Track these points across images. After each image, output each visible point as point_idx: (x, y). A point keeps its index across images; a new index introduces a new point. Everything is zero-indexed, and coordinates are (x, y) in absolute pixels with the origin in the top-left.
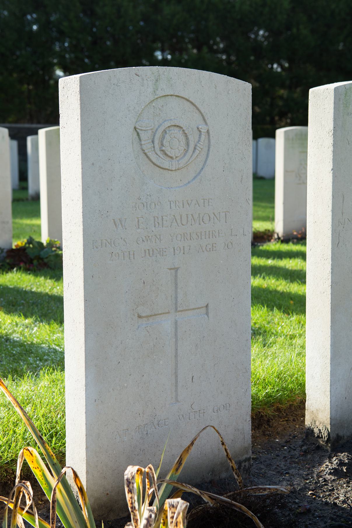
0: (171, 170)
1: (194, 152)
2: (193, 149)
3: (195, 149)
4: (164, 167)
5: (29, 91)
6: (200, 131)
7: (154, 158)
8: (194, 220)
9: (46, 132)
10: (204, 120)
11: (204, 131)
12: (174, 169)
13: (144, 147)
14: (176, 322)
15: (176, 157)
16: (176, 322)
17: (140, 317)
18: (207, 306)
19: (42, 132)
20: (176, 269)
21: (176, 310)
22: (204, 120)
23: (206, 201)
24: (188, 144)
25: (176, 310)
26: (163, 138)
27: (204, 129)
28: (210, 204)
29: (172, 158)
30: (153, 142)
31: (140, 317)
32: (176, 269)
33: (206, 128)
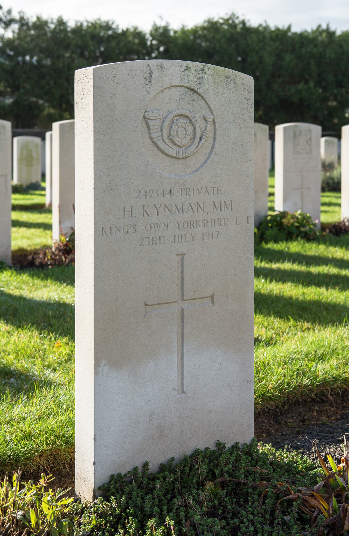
0: (179, 159)
1: (199, 143)
2: (199, 139)
3: (201, 140)
4: (169, 153)
5: (344, 467)
6: (206, 121)
7: (160, 143)
8: (178, 210)
9: (60, 125)
10: (211, 110)
11: (210, 120)
12: (181, 157)
13: (153, 136)
14: (183, 310)
15: (184, 146)
16: (183, 310)
17: (146, 305)
18: (212, 296)
19: (56, 126)
20: (183, 255)
21: (183, 300)
22: (211, 110)
23: (216, 189)
24: (194, 136)
25: (183, 300)
26: (171, 127)
27: (210, 118)
28: (219, 192)
29: (180, 147)
30: (161, 130)
31: (143, 206)
32: (183, 255)
33: (212, 117)
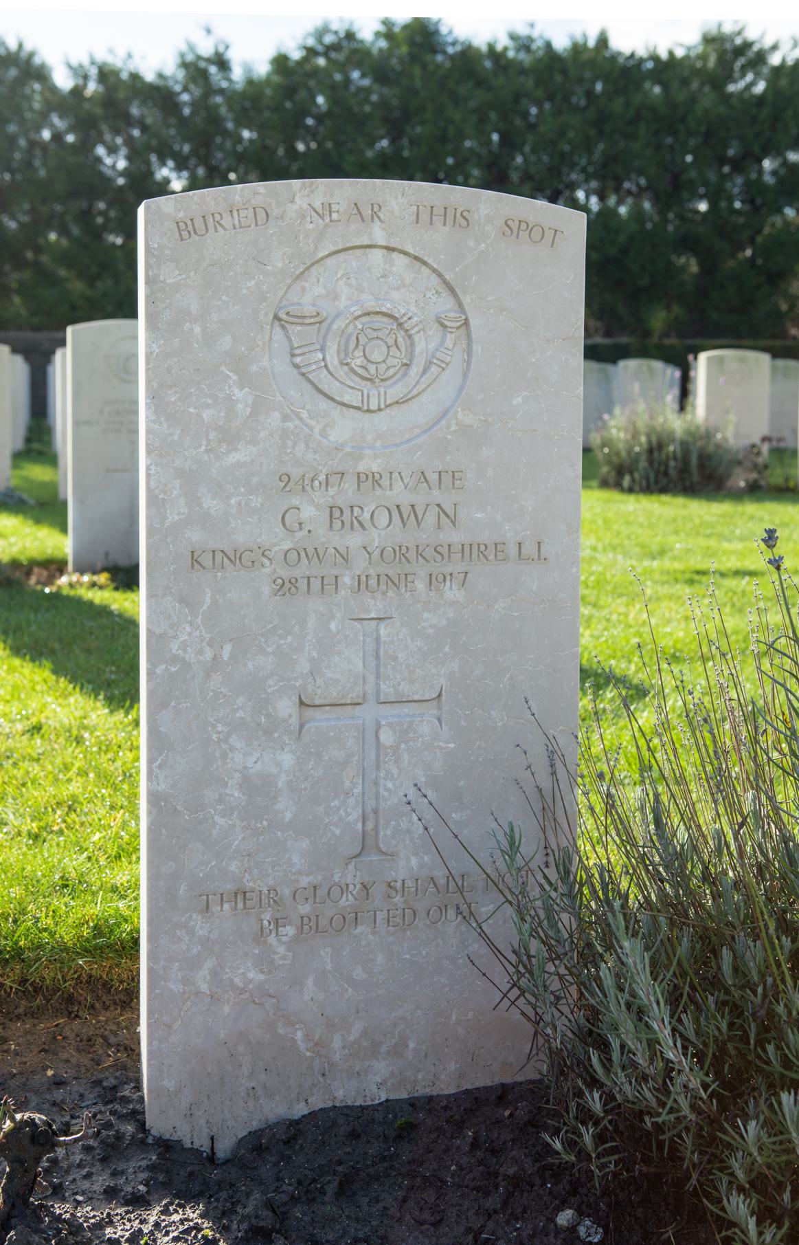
0: (369, 411)
